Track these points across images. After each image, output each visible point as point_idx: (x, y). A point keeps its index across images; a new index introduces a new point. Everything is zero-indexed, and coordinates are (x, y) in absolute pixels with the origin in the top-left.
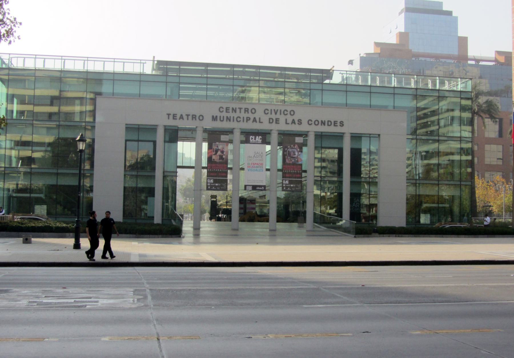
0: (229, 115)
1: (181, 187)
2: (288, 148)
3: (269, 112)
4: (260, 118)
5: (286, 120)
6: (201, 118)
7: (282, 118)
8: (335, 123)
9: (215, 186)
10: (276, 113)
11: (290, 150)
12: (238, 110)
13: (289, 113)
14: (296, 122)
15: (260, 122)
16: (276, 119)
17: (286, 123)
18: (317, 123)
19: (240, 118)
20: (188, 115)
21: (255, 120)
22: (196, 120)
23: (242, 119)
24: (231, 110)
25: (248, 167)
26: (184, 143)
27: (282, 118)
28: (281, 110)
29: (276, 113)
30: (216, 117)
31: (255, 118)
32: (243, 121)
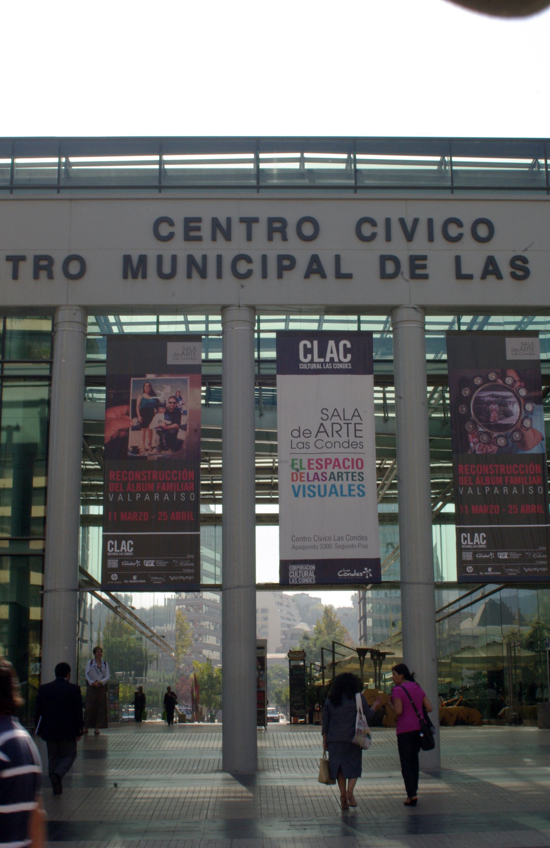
0: (197, 250)
1: (215, 642)
2: (474, 388)
3: (381, 230)
4: (338, 258)
5: (458, 259)
6: (76, 267)
7: (439, 257)
9: (143, 572)
10: (409, 236)
11: (486, 395)
12: (239, 230)
13: (466, 230)
14: (505, 269)
15: (339, 275)
16: (413, 259)
17: (460, 276)
19: (249, 260)
21: (315, 267)
22: (50, 276)
23: (256, 266)
24: (206, 230)
25: (297, 475)
26: (443, 526)
28: (430, 222)
29: (409, 236)
30: (143, 259)
31: (315, 259)
32: (264, 275)
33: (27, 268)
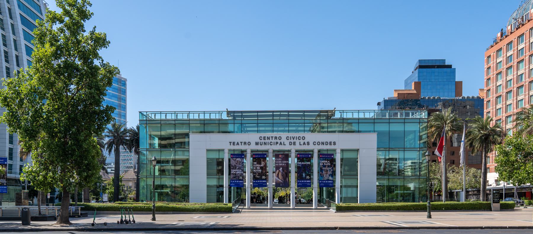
0: (265, 141)
6: (249, 144)
7: (297, 142)
8: (330, 143)
12: (271, 138)
14: (306, 143)
18: (319, 143)
20: (241, 143)
21: (281, 144)
27: (297, 142)
33: (232, 144)
